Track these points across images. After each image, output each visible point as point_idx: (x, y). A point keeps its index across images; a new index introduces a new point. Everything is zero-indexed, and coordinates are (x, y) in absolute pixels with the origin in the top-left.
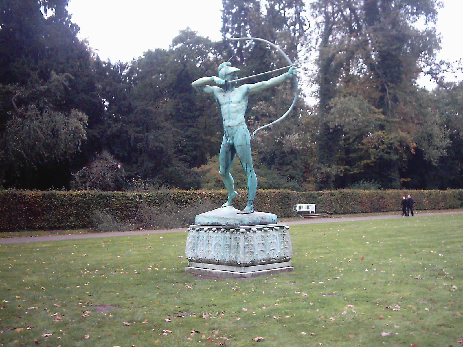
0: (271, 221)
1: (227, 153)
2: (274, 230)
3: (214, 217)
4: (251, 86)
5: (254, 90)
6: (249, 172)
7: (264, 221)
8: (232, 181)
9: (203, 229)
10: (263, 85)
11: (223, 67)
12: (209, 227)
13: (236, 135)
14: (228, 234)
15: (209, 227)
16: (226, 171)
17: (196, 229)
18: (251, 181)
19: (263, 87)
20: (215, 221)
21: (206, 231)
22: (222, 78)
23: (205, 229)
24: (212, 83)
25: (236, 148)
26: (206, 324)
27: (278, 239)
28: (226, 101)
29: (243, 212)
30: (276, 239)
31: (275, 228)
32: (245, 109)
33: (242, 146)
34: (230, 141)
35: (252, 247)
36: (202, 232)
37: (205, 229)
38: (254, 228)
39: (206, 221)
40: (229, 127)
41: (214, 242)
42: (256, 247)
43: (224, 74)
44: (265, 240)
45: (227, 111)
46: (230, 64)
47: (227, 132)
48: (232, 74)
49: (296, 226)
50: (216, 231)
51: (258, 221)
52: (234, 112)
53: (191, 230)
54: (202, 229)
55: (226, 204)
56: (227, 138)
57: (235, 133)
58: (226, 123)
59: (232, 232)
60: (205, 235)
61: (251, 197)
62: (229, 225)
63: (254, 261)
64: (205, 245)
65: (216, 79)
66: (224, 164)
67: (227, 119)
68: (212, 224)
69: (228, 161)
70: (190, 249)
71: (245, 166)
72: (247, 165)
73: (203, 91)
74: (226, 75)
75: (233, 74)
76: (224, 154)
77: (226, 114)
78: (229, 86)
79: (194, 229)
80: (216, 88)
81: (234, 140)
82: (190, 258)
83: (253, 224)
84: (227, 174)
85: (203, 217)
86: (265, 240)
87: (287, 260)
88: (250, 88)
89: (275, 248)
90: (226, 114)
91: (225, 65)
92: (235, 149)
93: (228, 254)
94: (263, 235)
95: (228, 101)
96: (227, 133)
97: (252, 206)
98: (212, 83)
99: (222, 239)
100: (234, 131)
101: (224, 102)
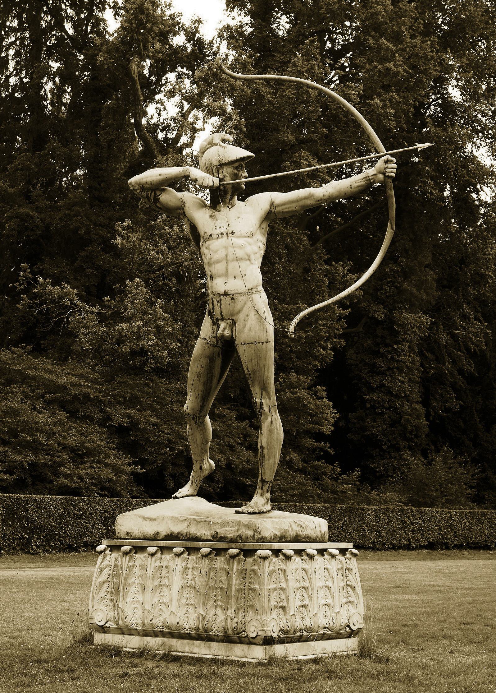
0: (319, 534)
1: (211, 359)
2: (327, 557)
3: (175, 519)
4: (279, 197)
5: (285, 208)
6: (266, 410)
7: (304, 533)
10: (310, 196)
12: (162, 543)
13: (242, 316)
14: (220, 562)
15: (162, 543)
18: (270, 431)
19: (309, 202)
20: (177, 529)
21: (152, 555)
22: (209, 170)
25: (241, 350)
27: (335, 580)
28: (219, 231)
30: (330, 580)
31: (330, 551)
32: (262, 252)
33: (255, 343)
34: (224, 329)
35: (283, 596)
37: (152, 549)
38: (288, 548)
39: (150, 529)
40: (225, 294)
41: (177, 583)
42: (291, 596)
43: (216, 163)
44: (310, 579)
45: (221, 254)
47: (217, 308)
48: (237, 164)
50: (159, 555)
51: (292, 533)
53: (108, 552)
56: (215, 323)
57: (239, 311)
59: (233, 557)
60: (152, 564)
62: (223, 539)
64: (149, 588)
67: (220, 276)
68: (171, 537)
69: (211, 382)
70: (103, 599)
71: (259, 394)
72: (264, 393)
73: (157, 200)
74: (221, 165)
75: (237, 164)
76: (204, 362)
77: (218, 262)
79: (113, 548)
81: (237, 328)
83: (282, 539)
85: (140, 520)
86: (310, 579)
87: (352, 634)
90: (218, 262)
93: (191, 610)
94: (306, 566)
95: (224, 230)
97: (268, 495)
99: (203, 573)
100: (238, 306)
101: (215, 232)
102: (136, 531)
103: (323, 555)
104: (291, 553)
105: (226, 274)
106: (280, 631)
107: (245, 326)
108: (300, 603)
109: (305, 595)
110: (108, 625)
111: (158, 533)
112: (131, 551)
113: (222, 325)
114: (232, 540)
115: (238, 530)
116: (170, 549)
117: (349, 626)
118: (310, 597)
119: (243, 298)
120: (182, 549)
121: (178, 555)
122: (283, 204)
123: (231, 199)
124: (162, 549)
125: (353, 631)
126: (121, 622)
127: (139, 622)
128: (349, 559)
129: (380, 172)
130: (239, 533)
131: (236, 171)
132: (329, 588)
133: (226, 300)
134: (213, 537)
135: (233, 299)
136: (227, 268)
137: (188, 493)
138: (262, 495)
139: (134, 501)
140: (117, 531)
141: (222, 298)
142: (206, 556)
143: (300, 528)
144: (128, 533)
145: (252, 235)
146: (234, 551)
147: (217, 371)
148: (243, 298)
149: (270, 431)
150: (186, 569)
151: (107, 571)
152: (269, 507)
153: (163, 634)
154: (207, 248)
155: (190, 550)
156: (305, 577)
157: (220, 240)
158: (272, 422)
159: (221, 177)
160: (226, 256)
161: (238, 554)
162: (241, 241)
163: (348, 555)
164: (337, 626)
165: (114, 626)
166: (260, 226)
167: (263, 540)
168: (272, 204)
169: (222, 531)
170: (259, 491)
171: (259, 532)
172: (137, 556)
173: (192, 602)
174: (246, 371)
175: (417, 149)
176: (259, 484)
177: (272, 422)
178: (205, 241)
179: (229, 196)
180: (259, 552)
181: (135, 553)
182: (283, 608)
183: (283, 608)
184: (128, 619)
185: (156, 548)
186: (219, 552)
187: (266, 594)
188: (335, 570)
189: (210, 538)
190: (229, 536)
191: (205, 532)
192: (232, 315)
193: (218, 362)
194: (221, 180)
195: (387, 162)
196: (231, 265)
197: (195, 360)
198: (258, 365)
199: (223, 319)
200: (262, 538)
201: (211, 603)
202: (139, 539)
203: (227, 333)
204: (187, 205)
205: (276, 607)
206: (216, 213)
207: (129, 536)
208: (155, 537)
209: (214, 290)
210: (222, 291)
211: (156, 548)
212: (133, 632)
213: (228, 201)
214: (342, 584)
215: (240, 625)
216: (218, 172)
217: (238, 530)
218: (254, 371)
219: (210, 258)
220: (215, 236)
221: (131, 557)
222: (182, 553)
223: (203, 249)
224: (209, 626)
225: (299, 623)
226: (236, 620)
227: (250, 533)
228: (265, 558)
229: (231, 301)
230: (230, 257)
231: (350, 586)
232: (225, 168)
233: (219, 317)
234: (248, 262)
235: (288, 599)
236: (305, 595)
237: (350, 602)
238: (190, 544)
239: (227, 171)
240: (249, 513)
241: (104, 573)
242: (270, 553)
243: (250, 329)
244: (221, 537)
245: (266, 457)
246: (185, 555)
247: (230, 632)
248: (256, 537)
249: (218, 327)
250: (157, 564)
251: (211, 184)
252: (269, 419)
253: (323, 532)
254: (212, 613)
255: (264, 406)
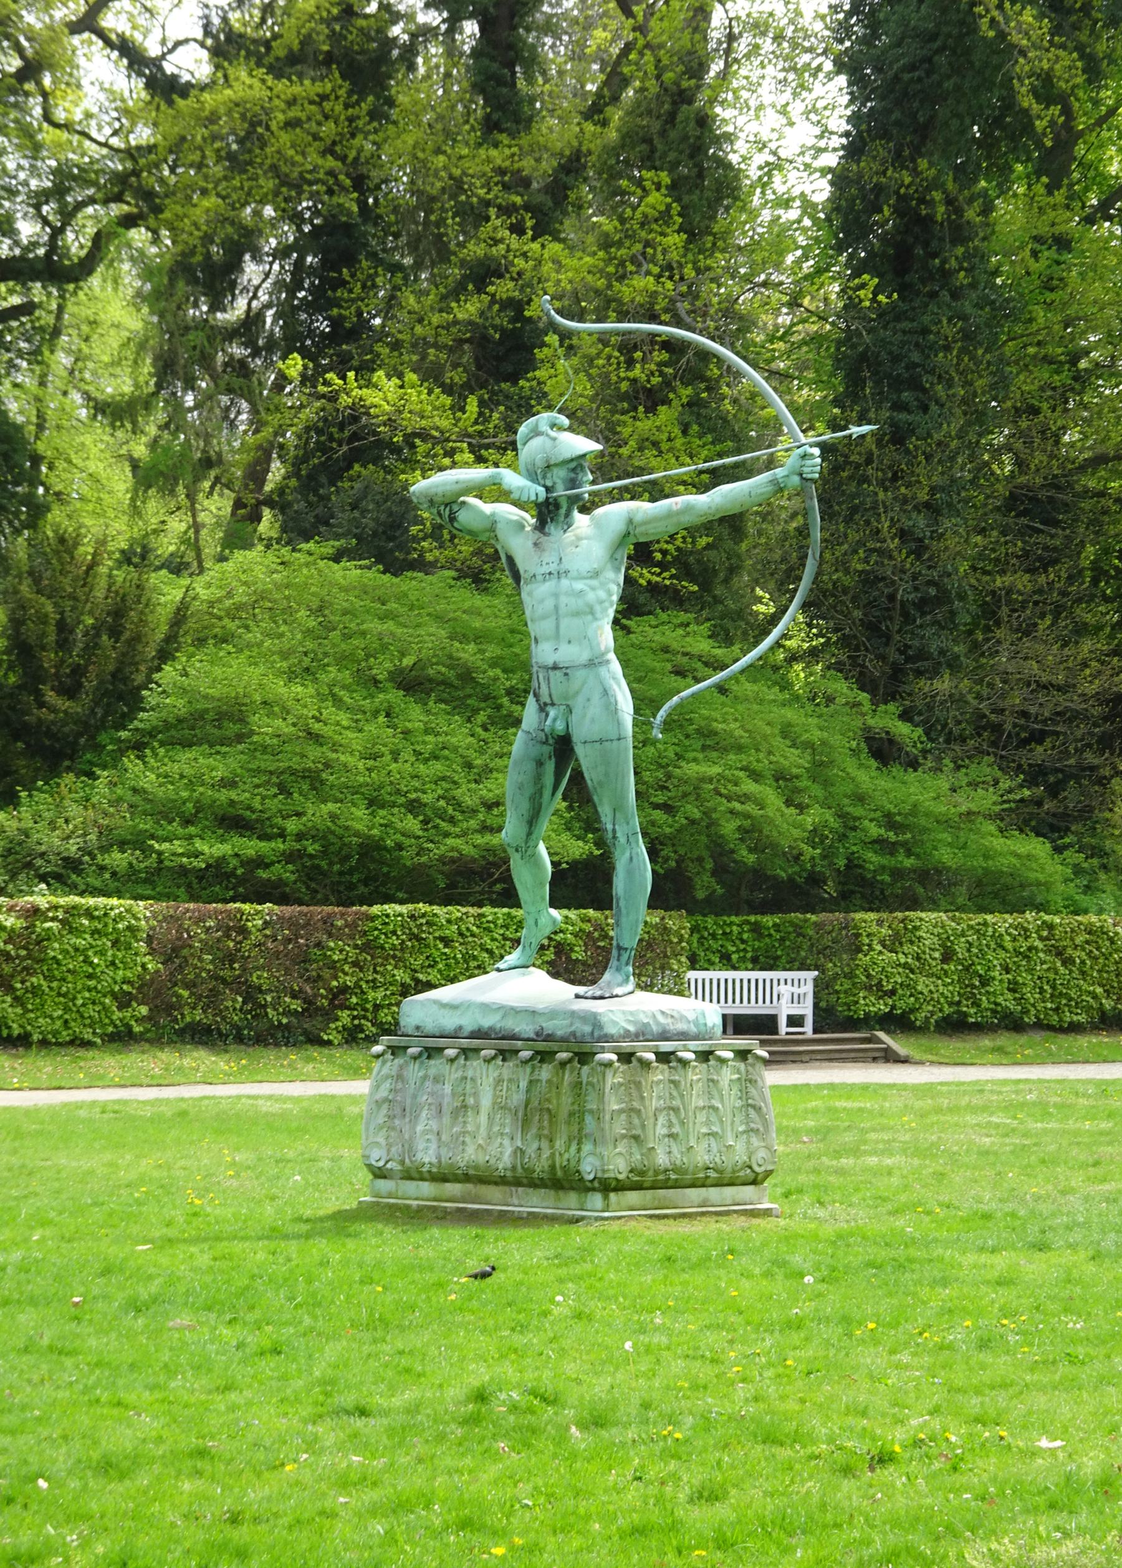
3: (485, 1007)
4: (643, 508)
6: (622, 839)
8: (545, 869)
9: (440, 1050)
10: (688, 509)
11: (536, 433)
14: (546, 1072)
16: (529, 834)
17: (410, 1050)
18: (630, 873)
21: (452, 1061)
22: (532, 476)
23: (451, 1052)
24: (501, 494)
25: (580, 750)
26: (288, 1468)
28: (545, 569)
29: (598, 993)
31: (680, 1054)
33: (601, 741)
34: (555, 720)
36: (436, 1066)
37: (451, 1052)
39: (449, 1022)
40: (555, 667)
43: (540, 463)
46: (566, 422)
47: (544, 686)
48: (573, 465)
49: (1005, 1082)
52: (577, 614)
53: (389, 1056)
54: (432, 1052)
55: (513, 958)
56: (543, 708)
57: (577, 693)
58: (544, 653)
59: (563, 1064)
60: (453, 1074)
61: (630, 940)
62: (549, 1038)
63: (642, 1173)
65: (512, 479)
66: (525, 806)
67: (547, 639)
68: (478, 1034)
69: (541, 796)
75: (576, 464)
77: (544, 617)
78: (557, 506)
80: (506, 511)
81: (574, 719)
82: (381, 1164)
84: (531, 843)
85: (435, 1007)
88: (639, 518)
89: (714, 1129)
91: (544, 427)
92: (572, 750)
95: (553, 568)
96: (544, 690)
98: (497, 493)
102: (430, 1026)
103: (707, 1060)
104: (651, 1056)
105: (557, 636)
106: (631, 1171)
107: (584, 716)
108: (665, 1131)
109: (674, 1120)
110: (389, 1166)
111: (460, 1028)
112: (420, 1054)
113: (552, 713)
114: (563, 1040)
115: (571, 1025)
116: (477, 1050)
117: (750, 1167)
118: (682, 1123)
119: (580, 674)
120: (493, 1052)
121: (488, 1061)
122: (645, 523)
123: (568, 514)
124: (465, 1052)
125: (757, 1174)
126: (407, 1161)
127: (434, 1161)
128: (753, 1065)
129: (794, 473)
130: (573, 1029)
131: (573, 475)
132: (716, 1109)
133: (556, 676)
134: (537, 1034)
135: (566, 674)
136: (557, 627)
137: (518, 963)
138: (618, 969)
139: (82, 1113)
140: (402, 1023)
141: (551, 673)
142: (415, 1058)
143: (670, 1020)
144: (418, 1028)
145: (596, 574)
146: (563, 1056)
147: (549, 779)
148: (580, 674)
149: (630, 873)
150: (499, 1081)
151: (387, 1085)
152: (630, 986)
153: (466, 1178)
154: (530, 594)
155: (505, 1054)
156: (675, 1093)
157: (547, 584)
158: (631, 859)
159: (549, 483)
160: (556, 608)
161: (570, 1061)
162: (579, 585)
163: (750, 1060)
164: (728, 1165)
165: (399, 1168)
166: (612, 558)
167: (607, 1038)
168: (630, 521)
169: (549, 1026)
170: (613, 963)
171: (601, 1027)
172: (432, 1062)
173: (507, 1130)
174: (589, 782)
175: (850, 436)
176: (615, 952)
177: (631, 859)
178: (526, 583)
179: (563, 511)
180: (598, 1057)
181: (429, 1057)
182: (636, 1138)
183: (636, 1138)
184: (419, 1156)
185: (456, 1051)
186: (544, 1056)
187: (608, 1117)
188: (727, 1083)
189: (532, 1035)
190: (559, 1033)
191: (526, 1028)
192: (566, 698)
193: (550, 767)
194: (548, 490)
195: (804, 456)
196: (565, 623)
197: (515, 763)
198: (606, 774)
199: (553, 704)
200: (606, 1035)
201: (534, 1131)
202: (932, 1063)
203: (560, 727)
204: (499, 526)
205: (624, 1136)
206: (544, 539)
207: (420, 1032)
208: (455, 1035)
209: (540, 661)
210: (550, 663)
211: (456, 1051)
212: (427, 1175)
213: (562, 518)
214: (739, 1103)
215: (573, 1163)
216: (544, 477)
217: (571, 1025)
218: (600, 784)
219: (533, 611)
220: (539, 578)
221: (422, 1063)
222: (456, 1058)
223: (524, 595)
224: (531, 1165)
225: (662, 1159)
226: (566, 1156)
227: (587, 1029)
228: (609, 1064)
229: (563, 679)
230: (563, 610)
231: (753, 1107)
232: (555, 470)
233: (548, 701)
234: (590, 617)
235: (643, 1126)
236: (674, 1120)
237: (752, 1130)
238: (505, 1044)
239: (559, 476)
240: (595, 998)
241: (383, 1087)
242: (614, 1057)
243: (593, 720)
244: (549, 1035)
245: (624, 911)
246: (499, 1062)
247: (559, 1173)
248: (596, 1034)
249: (547, 715)
250: (459, 1074)
251: (533, 498)
252: (627, 855)
253: (710, 1024)
254: (535, 1145)
255: (618, 834)
